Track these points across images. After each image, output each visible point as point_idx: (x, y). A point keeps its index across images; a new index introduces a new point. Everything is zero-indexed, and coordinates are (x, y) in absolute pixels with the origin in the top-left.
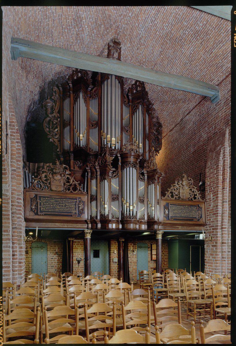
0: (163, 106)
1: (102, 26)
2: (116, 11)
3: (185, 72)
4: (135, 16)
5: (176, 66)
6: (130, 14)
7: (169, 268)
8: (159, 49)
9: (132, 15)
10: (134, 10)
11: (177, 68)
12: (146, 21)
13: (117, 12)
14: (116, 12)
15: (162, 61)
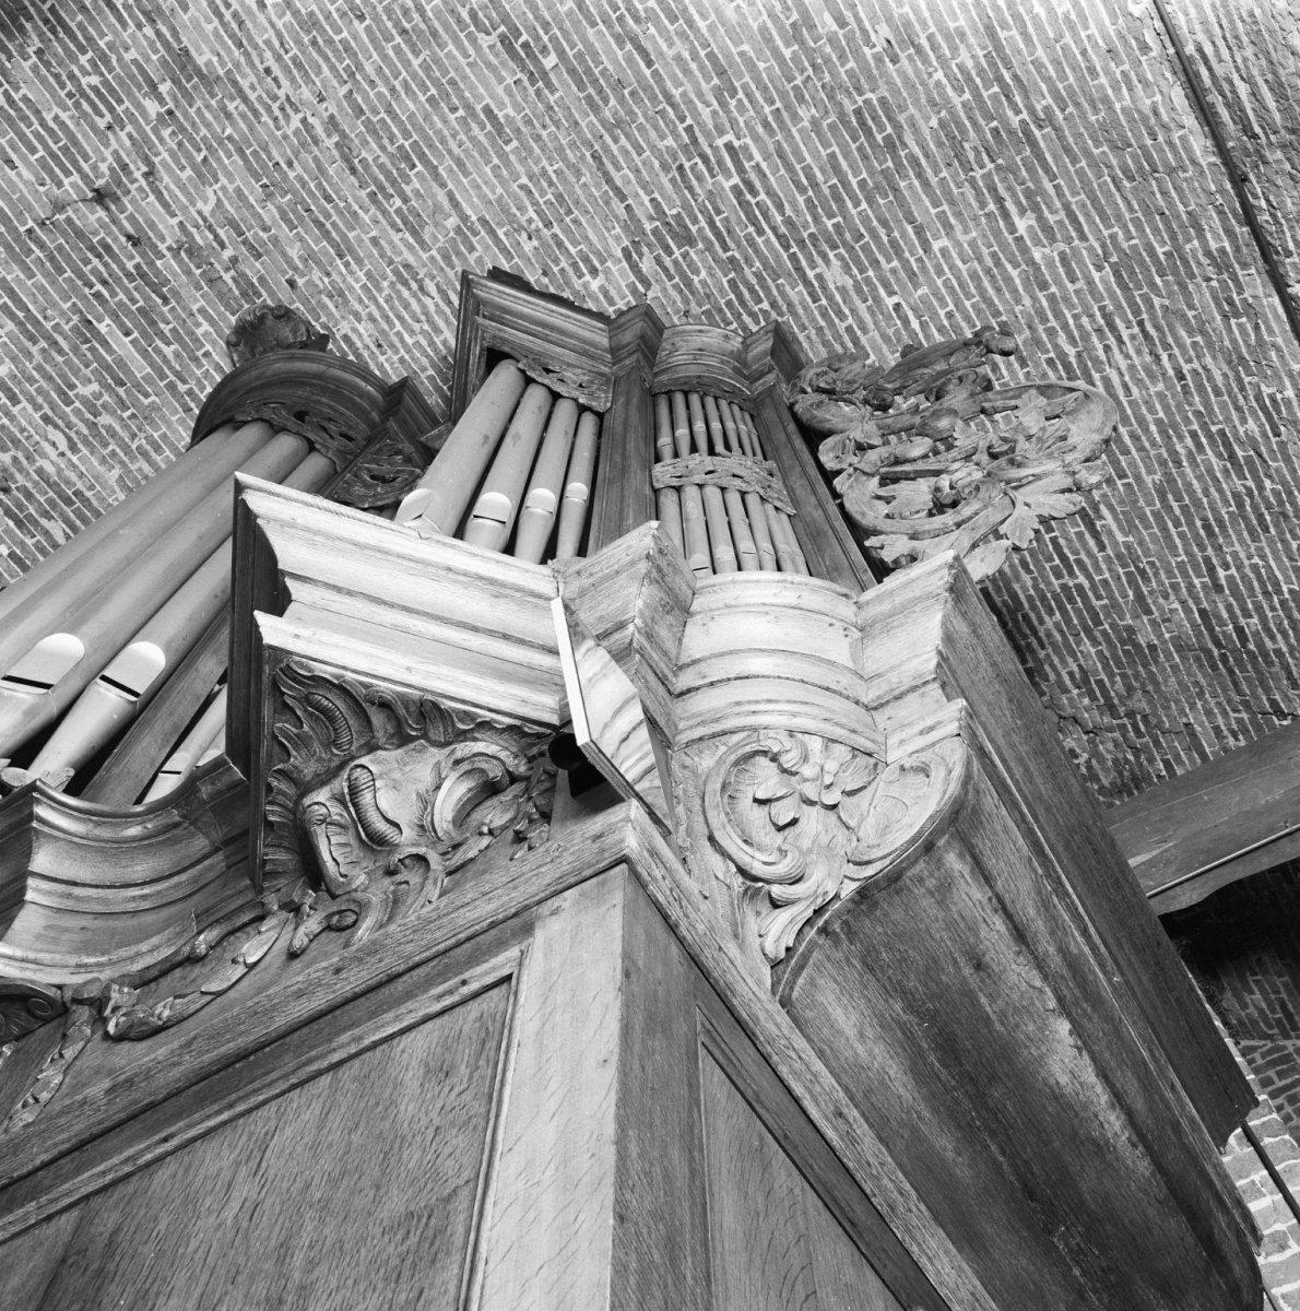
1: (102, 328)
2: (68, 173)
4: (176, 81)
6: (152, 108)
7: (303, 795)
8: (478, 48)
9: (162, 101)
10: (134, 61)
12: (235, 15)
13: (79, 170)
14: (76, 177)
15: (595, 82)
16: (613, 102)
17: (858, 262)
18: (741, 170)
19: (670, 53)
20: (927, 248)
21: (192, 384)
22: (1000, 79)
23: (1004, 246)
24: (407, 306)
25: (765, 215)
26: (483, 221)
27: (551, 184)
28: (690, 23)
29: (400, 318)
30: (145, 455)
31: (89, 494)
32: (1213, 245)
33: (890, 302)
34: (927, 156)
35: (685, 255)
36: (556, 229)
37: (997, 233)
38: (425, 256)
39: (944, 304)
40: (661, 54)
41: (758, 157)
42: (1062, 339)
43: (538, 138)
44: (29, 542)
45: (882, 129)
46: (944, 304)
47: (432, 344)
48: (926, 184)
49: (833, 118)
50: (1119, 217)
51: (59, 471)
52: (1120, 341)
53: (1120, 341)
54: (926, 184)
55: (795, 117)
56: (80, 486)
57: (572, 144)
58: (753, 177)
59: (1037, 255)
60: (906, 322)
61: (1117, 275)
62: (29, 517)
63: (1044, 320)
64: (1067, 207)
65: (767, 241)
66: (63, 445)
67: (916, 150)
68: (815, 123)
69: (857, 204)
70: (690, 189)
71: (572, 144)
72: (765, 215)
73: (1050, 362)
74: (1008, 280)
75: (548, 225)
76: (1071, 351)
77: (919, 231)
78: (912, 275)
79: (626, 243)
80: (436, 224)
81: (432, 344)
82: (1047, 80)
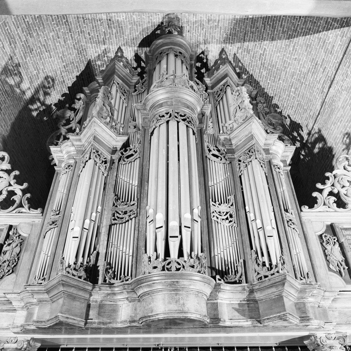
0: (282, 101)
3: (299, 22)
5: (279, 21)
11: (282, 23)
15: (254, 25)
16: (254, 29)
17: (269, 74)
18: (264, 52)
19: (268, 31)
20: (279, 80)
21: (153, 18)
22: (305, 76)
23: (288, 89)
24: (198, 30)
25: (262, 60)
26: (221, 28)
27: (236, 31)
28: (274, 31)
29: (195, 31)
30: (137, 26)
31: (124, 28)
32: (311, 114)
33: (268, 81)
34: (289, 73)
35: (246, 54)
36: (231, 37)
37: (289, 87)
38: (207, 25)
39: (275, 87)
40: (267, 30)
41: (268, 53)
42: (285, 103)
43: (239, 24)
44: (109, 31)
45: (286, 65)
46: (275, 87)
47: (197, 37)
48: (286, 75)
49: (282, 58)
50: (304, 100)
51: (121, 22)
52: (292, 109)
53: (292, 109)
54: (286, 75)
55: (277, 53)
56: (123, 26)
57: (243, 29)
58: (265, 54)
59: (291, 94)
60: (268, 85)
61: (298, 104)
62: (111, 27)
63: (285, 99)
64: (299, 93)
65: (259, 63)
66: (124, 17)
67: (288, 71)
68: (279, 56)
69: (275, 69)
70: (255, 48)
71: (243, 29)
72: (262, 60)
73: (282, 104)
74: (285, 92)
75: (230, 35)
76: (285, 105)
77: (280, 78)
78: (274, 81)
79: (239, 46)
80: (213, 22)
81: (197, 37)
82: (310, 82)
